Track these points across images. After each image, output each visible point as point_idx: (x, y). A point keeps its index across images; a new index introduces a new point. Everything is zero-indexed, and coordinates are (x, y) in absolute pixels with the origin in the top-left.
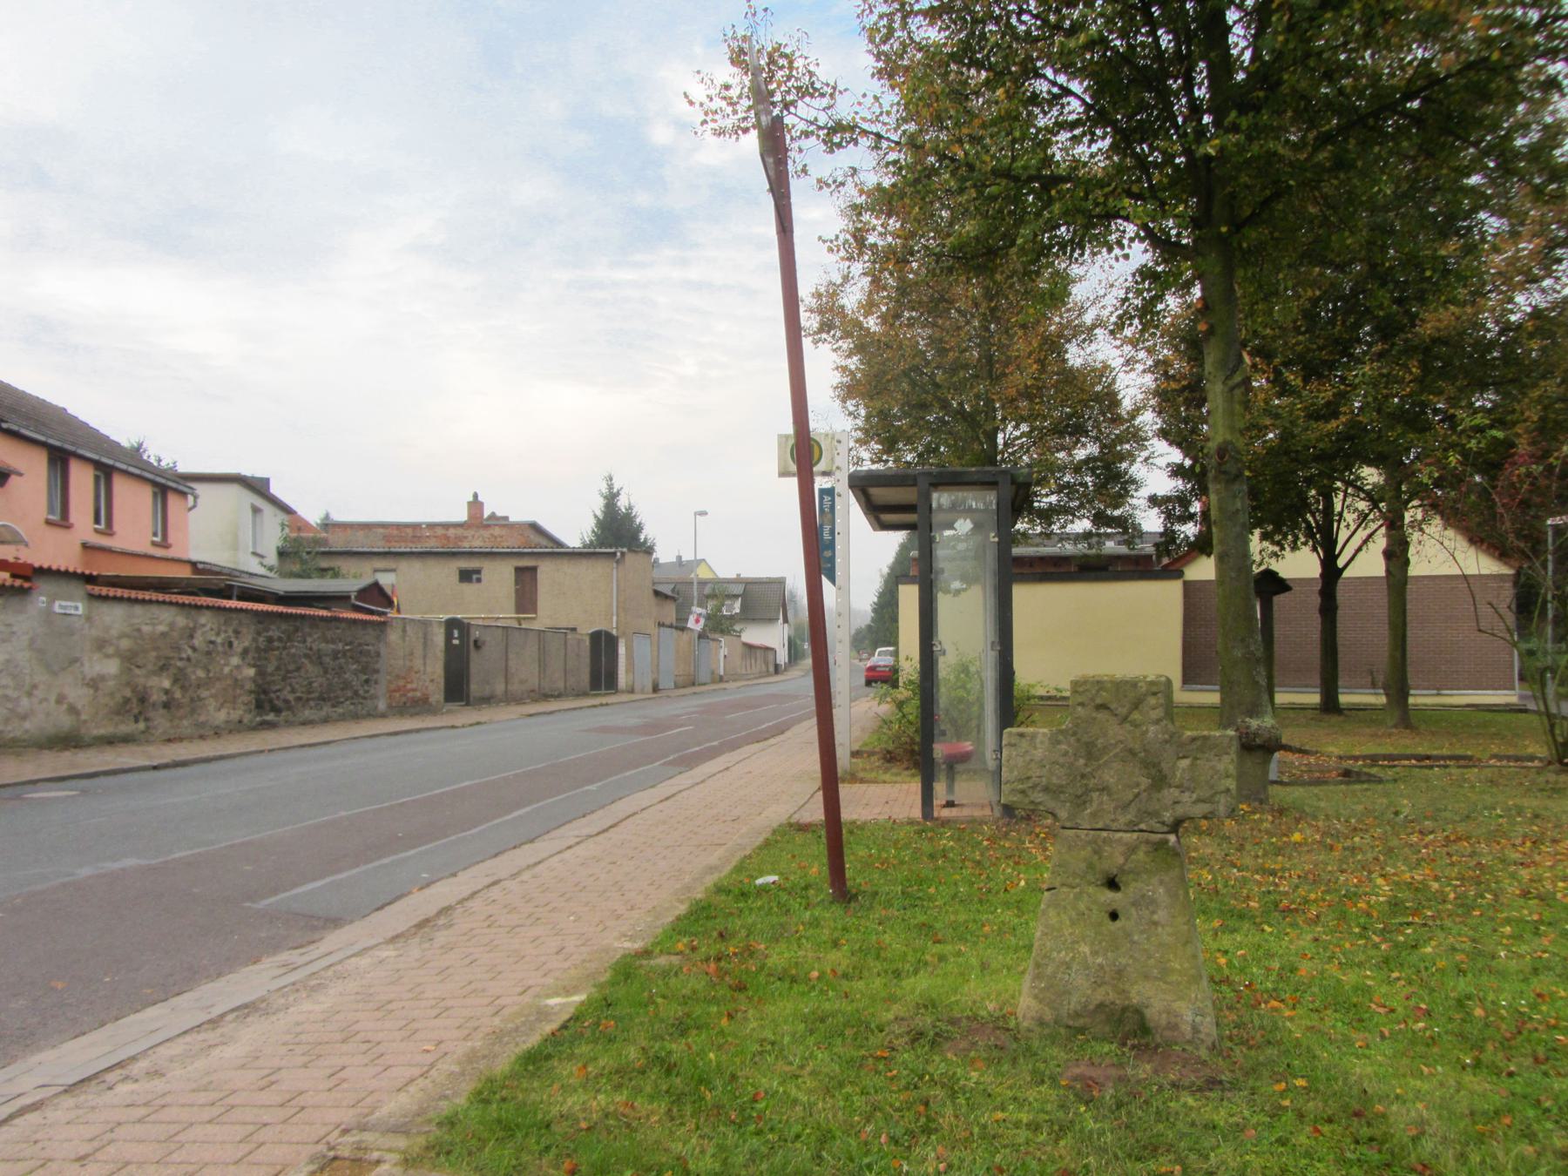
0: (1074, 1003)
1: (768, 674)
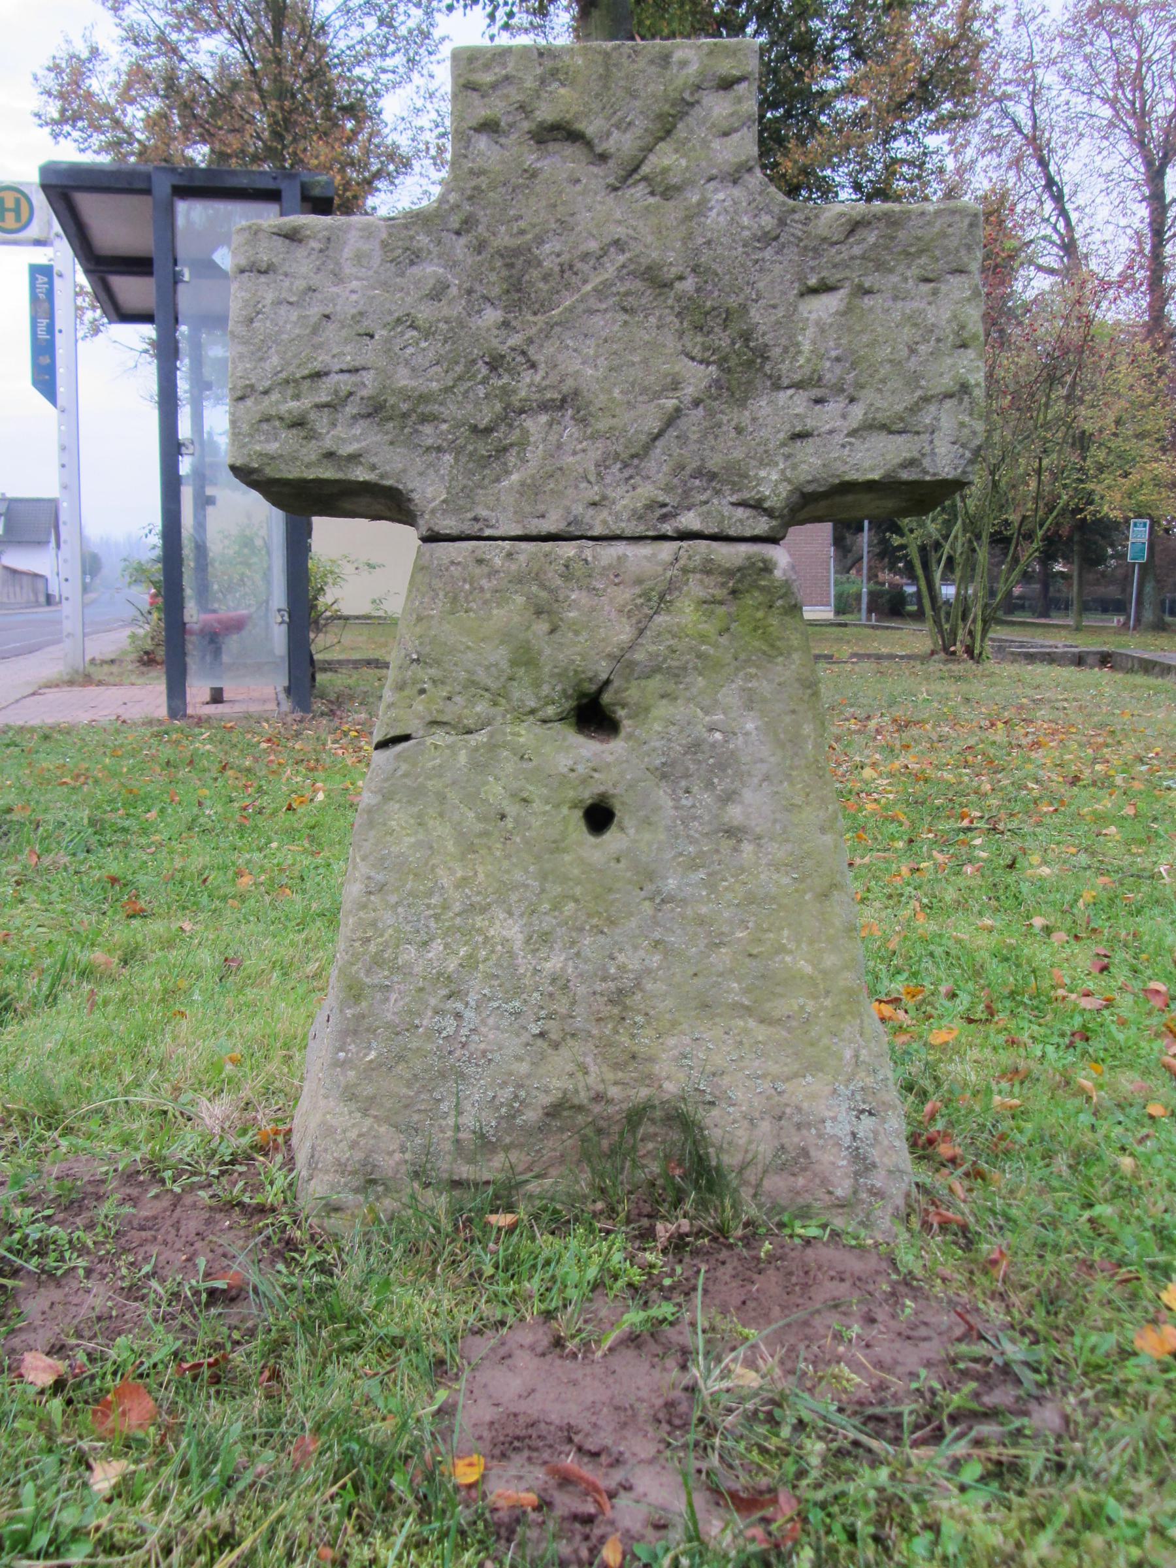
0: (475, 1107)
1: (37, 604)
